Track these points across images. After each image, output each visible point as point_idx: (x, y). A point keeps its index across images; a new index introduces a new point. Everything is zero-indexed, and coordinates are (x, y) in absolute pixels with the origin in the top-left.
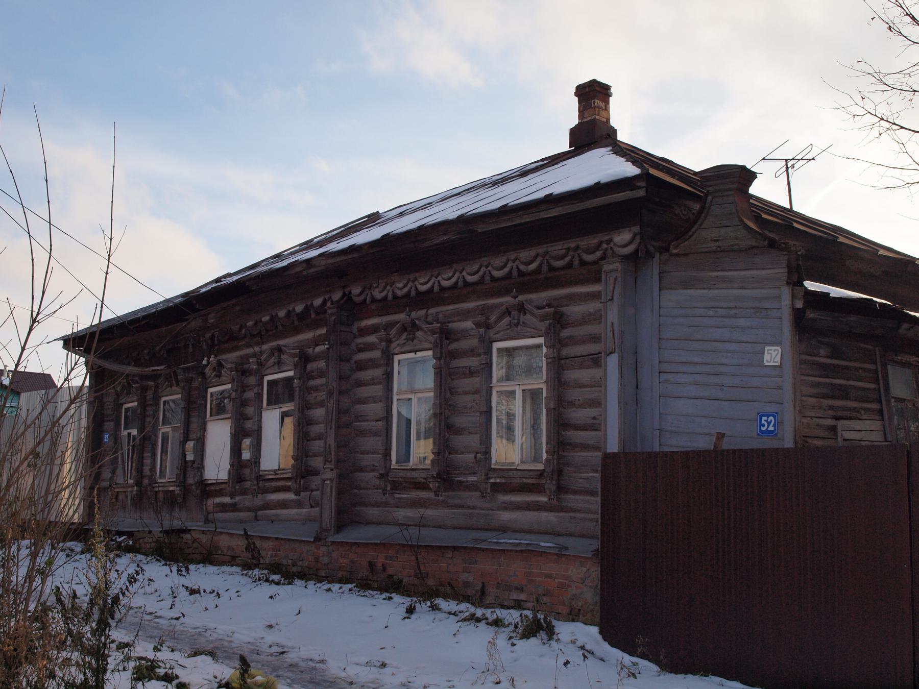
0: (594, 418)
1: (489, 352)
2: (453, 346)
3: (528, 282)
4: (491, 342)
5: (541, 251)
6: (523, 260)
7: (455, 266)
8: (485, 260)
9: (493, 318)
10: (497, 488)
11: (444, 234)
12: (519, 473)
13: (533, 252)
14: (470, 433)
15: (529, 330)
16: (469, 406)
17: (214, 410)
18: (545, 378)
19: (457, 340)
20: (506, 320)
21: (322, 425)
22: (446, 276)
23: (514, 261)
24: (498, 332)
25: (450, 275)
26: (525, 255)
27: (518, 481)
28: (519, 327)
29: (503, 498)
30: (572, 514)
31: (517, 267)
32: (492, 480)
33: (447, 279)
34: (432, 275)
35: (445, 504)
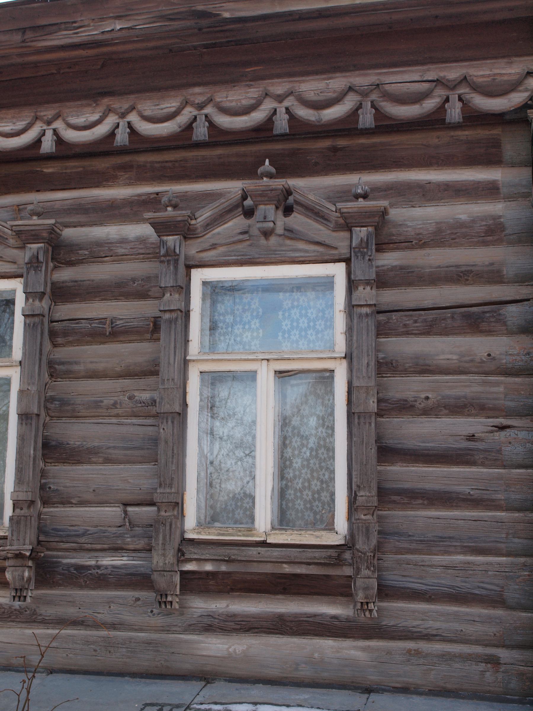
0: (471, 438)
1: (185, 290)
2: (65, 275)
3: (298, 147)
4: (189, 267)
5: (361, 80)
6: (311, 96)
7: (106, 101)
8: (198, 94)
9: (204, 215)
10: (193, 583)
11: (118, 17)
12: (276, 553)
13: (337, 83)
14: (108, 461)
15: (301, 245)
16: (107, 402)
17: (18, 228)
18: (17, 352)
19: (71, 264)
20: (237, 223)
21: (369, 616)
22: (80, 121)
23: (280, 99)
24: (214, 247)
25: (95, 117)
26: (312, 87)
27: (268, 569)
28: (273, 240)
29: (201, 605)
30: (411, 645)
31: (288, 110)
32: (190, 567)
33: (84, 125)
34: (37, 118)
35: (32, 618)
